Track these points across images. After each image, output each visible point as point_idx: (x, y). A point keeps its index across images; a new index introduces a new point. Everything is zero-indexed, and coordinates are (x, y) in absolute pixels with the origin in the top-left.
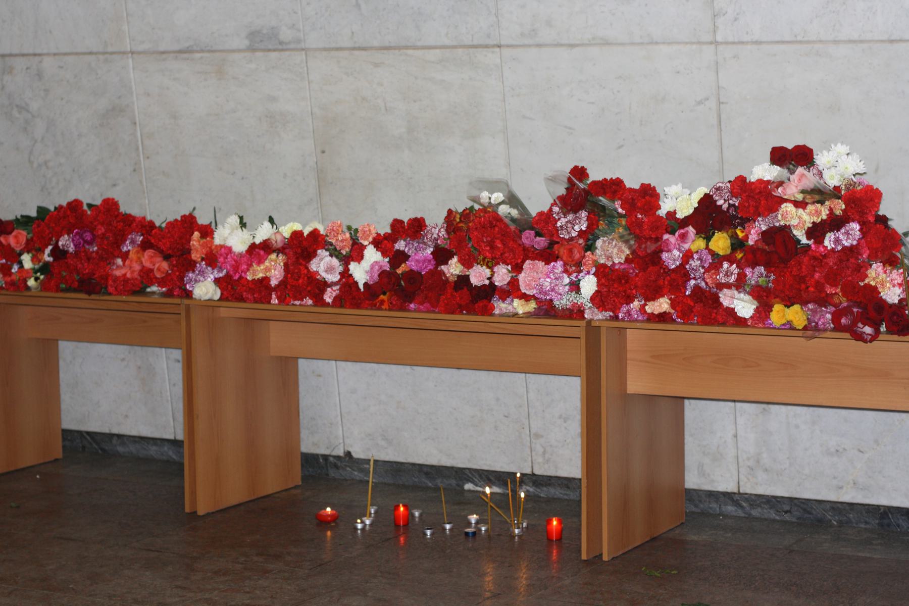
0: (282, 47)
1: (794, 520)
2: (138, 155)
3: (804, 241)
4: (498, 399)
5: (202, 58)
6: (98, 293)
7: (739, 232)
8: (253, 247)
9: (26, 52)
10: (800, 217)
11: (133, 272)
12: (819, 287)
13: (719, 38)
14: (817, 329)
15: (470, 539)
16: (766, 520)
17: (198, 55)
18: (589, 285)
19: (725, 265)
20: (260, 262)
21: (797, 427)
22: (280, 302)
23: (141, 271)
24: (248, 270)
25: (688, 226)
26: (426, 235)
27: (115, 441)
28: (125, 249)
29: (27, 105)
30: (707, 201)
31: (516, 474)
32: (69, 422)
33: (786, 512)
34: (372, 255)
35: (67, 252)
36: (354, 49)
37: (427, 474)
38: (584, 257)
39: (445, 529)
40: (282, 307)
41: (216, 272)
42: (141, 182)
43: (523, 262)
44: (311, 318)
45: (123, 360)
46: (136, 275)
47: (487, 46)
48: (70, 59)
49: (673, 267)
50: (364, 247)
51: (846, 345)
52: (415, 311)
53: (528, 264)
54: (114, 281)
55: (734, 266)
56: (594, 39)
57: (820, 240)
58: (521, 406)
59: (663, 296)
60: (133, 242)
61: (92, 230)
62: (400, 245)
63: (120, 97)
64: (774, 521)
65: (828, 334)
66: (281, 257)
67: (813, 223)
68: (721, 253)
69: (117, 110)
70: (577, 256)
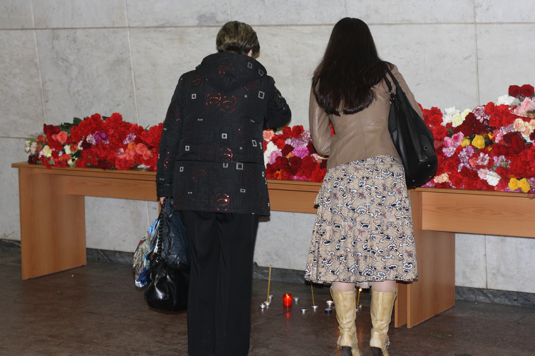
1: (519, 305)
2: (133, 88)
5: (170, 31)
6: (109, 168)
9: (66, 27)
11: (130, 156)
13: (478, 21)
16: (503, 305)
17: (168, 29)
19: (482, 155)
27: (117, 255)
28: (125, 143)
29: (67, 58)
30: (471, 117)
32: (90, 244)
35: (91, 144)
36: (261, 26)
42: (134, 103)
45: (122, 207)
46: (132, 158)
48: (92, 31)
49: (450, 156)
50: (267, 143)
52: (297, 180)
55: (487, 155)
56: (403, 20)
60: (130, 139)
62: (288, 142)
63: (122, 54)
64: (508, 305)
68: (479, 148)
69: (120, 61)
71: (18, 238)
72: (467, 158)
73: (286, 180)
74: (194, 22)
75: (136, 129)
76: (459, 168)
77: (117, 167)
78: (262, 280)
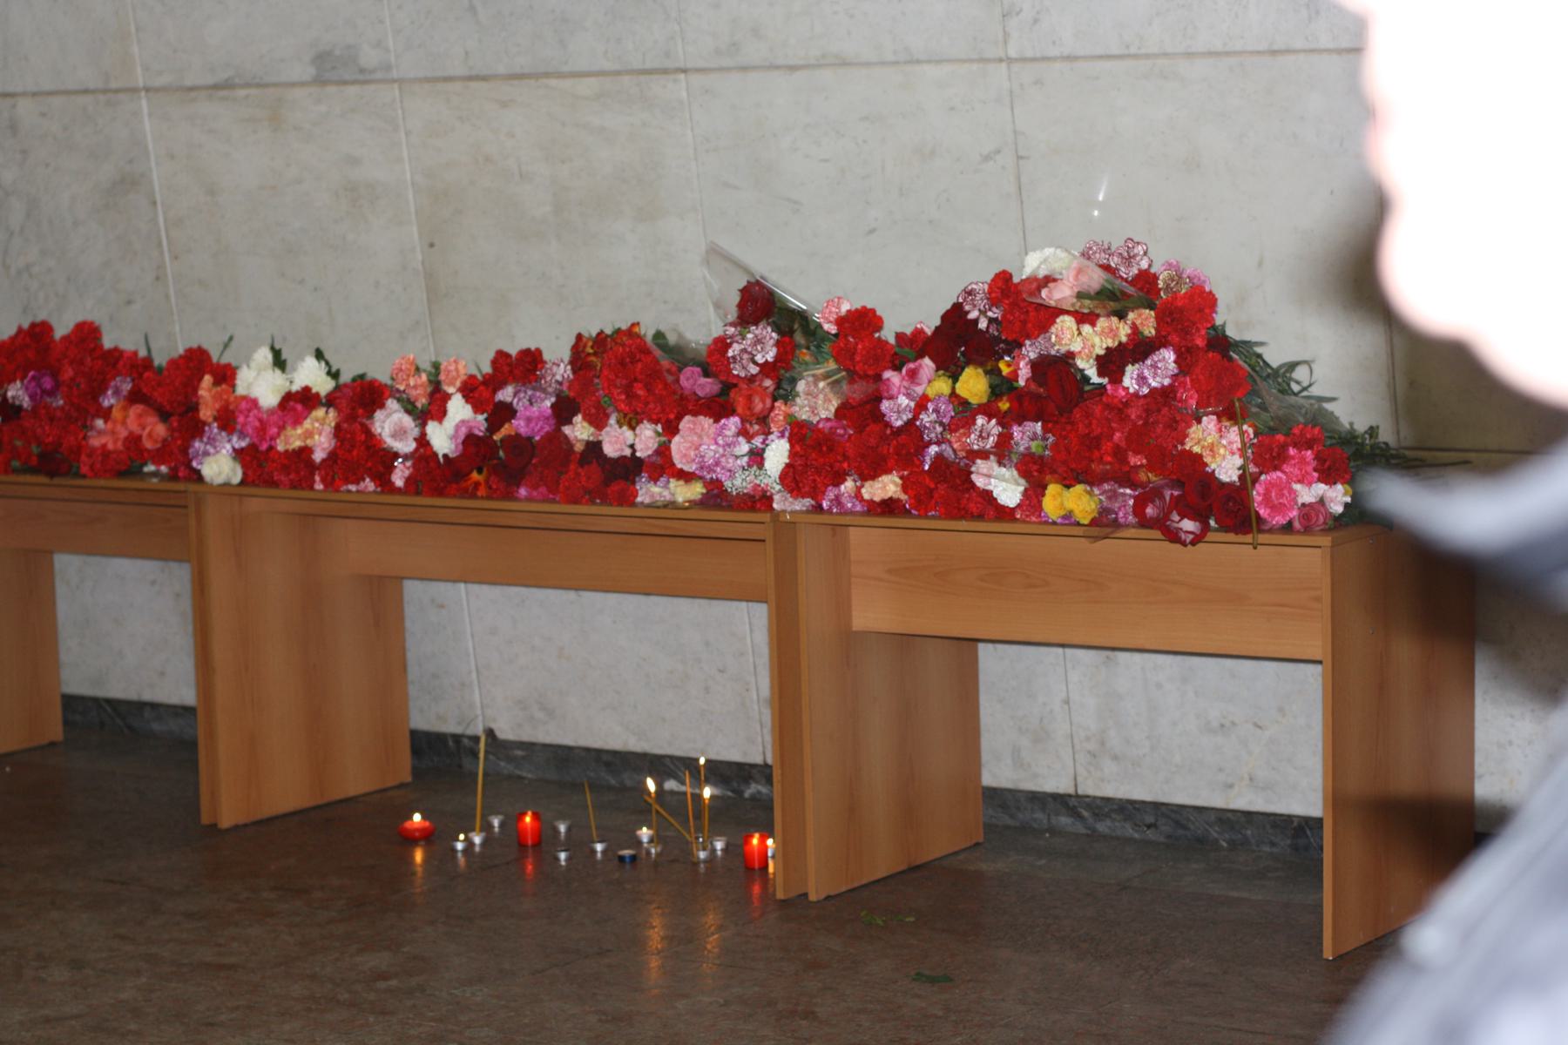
0: (364, 77)
1: (1162, 839)
2: (162, 253)
3: (1095, 379)
4: (707, 644)
5: (247, 96)
7: (1002, 365)
8: (288, 398)
10: (1085, 340)
11: (115, 442)
12: (1119, 454)
13: (1012, 53)
14: (1116, 524)
15: (628, 866)
16: (1118, 838)
17: (242, 93)
18: (778, 454)
19: (980, 420)
20: (298, 421)
21: (1159, 686)
22: (326, 486)
23: (126, 439)
24: (279, 434)
25: (922, 357)
26: (543, 377)
27: (147, 713)
28: (106, 403)
30: (955, 315)
31: (697, 760)
32: (76, 682)
33: (1149, 827)
34: (459, 410)
35: (20, 408)
36: (470, 78)
37: (608, 764)
38: (772, 408)
39: (594, 852)
40: (331, 496)
41: (235, 439)
42: (167, 297)
43: (680, 418)
44: (694, 529)
45: (153, 583)
46: (120, 445)
47: (665, 71)
48: (57, 101)
49: (899, 423)
51: (1154, 548)
53: (686, 423)
54: (90, 456)
55: (994, 421)
57: (1117, 378)
58: (742, 654)
59: (888, 471)
60: (117, 392)
61: (55, 375)
62: (506, 394)
63: (131, 162)
64: (1130, 840)
65: (1132, 532)
66: (332, 413)
67: (1108, 349)
68: (974, 401)
69: (129, 182)
70: (758, 406)
71: (178, 689)
72: (939, 429)
73: (498, 499)
74: (305, 71)
75: (132, 366)
76: (928, 459)
77: (85, 470)
78: (510, 777)
